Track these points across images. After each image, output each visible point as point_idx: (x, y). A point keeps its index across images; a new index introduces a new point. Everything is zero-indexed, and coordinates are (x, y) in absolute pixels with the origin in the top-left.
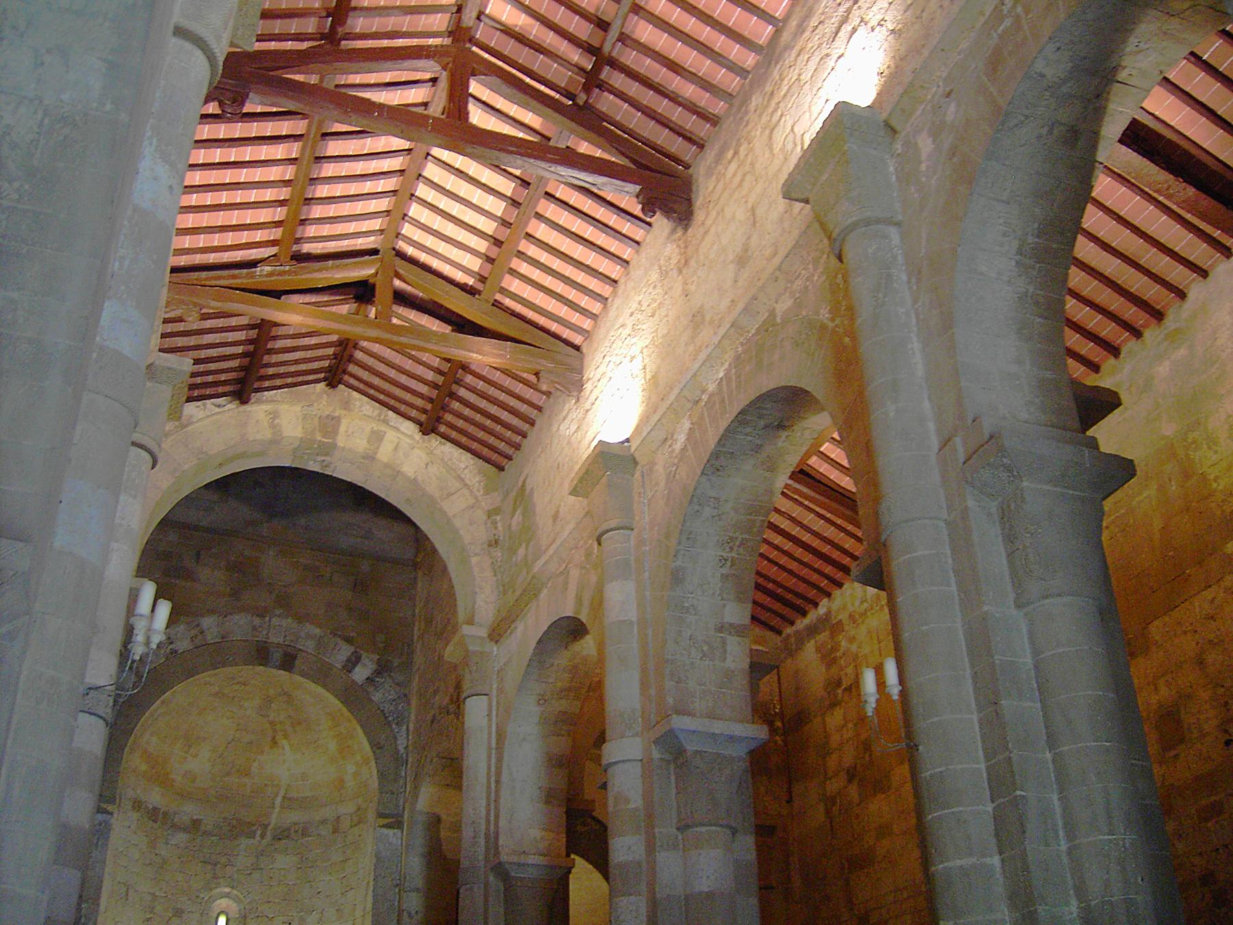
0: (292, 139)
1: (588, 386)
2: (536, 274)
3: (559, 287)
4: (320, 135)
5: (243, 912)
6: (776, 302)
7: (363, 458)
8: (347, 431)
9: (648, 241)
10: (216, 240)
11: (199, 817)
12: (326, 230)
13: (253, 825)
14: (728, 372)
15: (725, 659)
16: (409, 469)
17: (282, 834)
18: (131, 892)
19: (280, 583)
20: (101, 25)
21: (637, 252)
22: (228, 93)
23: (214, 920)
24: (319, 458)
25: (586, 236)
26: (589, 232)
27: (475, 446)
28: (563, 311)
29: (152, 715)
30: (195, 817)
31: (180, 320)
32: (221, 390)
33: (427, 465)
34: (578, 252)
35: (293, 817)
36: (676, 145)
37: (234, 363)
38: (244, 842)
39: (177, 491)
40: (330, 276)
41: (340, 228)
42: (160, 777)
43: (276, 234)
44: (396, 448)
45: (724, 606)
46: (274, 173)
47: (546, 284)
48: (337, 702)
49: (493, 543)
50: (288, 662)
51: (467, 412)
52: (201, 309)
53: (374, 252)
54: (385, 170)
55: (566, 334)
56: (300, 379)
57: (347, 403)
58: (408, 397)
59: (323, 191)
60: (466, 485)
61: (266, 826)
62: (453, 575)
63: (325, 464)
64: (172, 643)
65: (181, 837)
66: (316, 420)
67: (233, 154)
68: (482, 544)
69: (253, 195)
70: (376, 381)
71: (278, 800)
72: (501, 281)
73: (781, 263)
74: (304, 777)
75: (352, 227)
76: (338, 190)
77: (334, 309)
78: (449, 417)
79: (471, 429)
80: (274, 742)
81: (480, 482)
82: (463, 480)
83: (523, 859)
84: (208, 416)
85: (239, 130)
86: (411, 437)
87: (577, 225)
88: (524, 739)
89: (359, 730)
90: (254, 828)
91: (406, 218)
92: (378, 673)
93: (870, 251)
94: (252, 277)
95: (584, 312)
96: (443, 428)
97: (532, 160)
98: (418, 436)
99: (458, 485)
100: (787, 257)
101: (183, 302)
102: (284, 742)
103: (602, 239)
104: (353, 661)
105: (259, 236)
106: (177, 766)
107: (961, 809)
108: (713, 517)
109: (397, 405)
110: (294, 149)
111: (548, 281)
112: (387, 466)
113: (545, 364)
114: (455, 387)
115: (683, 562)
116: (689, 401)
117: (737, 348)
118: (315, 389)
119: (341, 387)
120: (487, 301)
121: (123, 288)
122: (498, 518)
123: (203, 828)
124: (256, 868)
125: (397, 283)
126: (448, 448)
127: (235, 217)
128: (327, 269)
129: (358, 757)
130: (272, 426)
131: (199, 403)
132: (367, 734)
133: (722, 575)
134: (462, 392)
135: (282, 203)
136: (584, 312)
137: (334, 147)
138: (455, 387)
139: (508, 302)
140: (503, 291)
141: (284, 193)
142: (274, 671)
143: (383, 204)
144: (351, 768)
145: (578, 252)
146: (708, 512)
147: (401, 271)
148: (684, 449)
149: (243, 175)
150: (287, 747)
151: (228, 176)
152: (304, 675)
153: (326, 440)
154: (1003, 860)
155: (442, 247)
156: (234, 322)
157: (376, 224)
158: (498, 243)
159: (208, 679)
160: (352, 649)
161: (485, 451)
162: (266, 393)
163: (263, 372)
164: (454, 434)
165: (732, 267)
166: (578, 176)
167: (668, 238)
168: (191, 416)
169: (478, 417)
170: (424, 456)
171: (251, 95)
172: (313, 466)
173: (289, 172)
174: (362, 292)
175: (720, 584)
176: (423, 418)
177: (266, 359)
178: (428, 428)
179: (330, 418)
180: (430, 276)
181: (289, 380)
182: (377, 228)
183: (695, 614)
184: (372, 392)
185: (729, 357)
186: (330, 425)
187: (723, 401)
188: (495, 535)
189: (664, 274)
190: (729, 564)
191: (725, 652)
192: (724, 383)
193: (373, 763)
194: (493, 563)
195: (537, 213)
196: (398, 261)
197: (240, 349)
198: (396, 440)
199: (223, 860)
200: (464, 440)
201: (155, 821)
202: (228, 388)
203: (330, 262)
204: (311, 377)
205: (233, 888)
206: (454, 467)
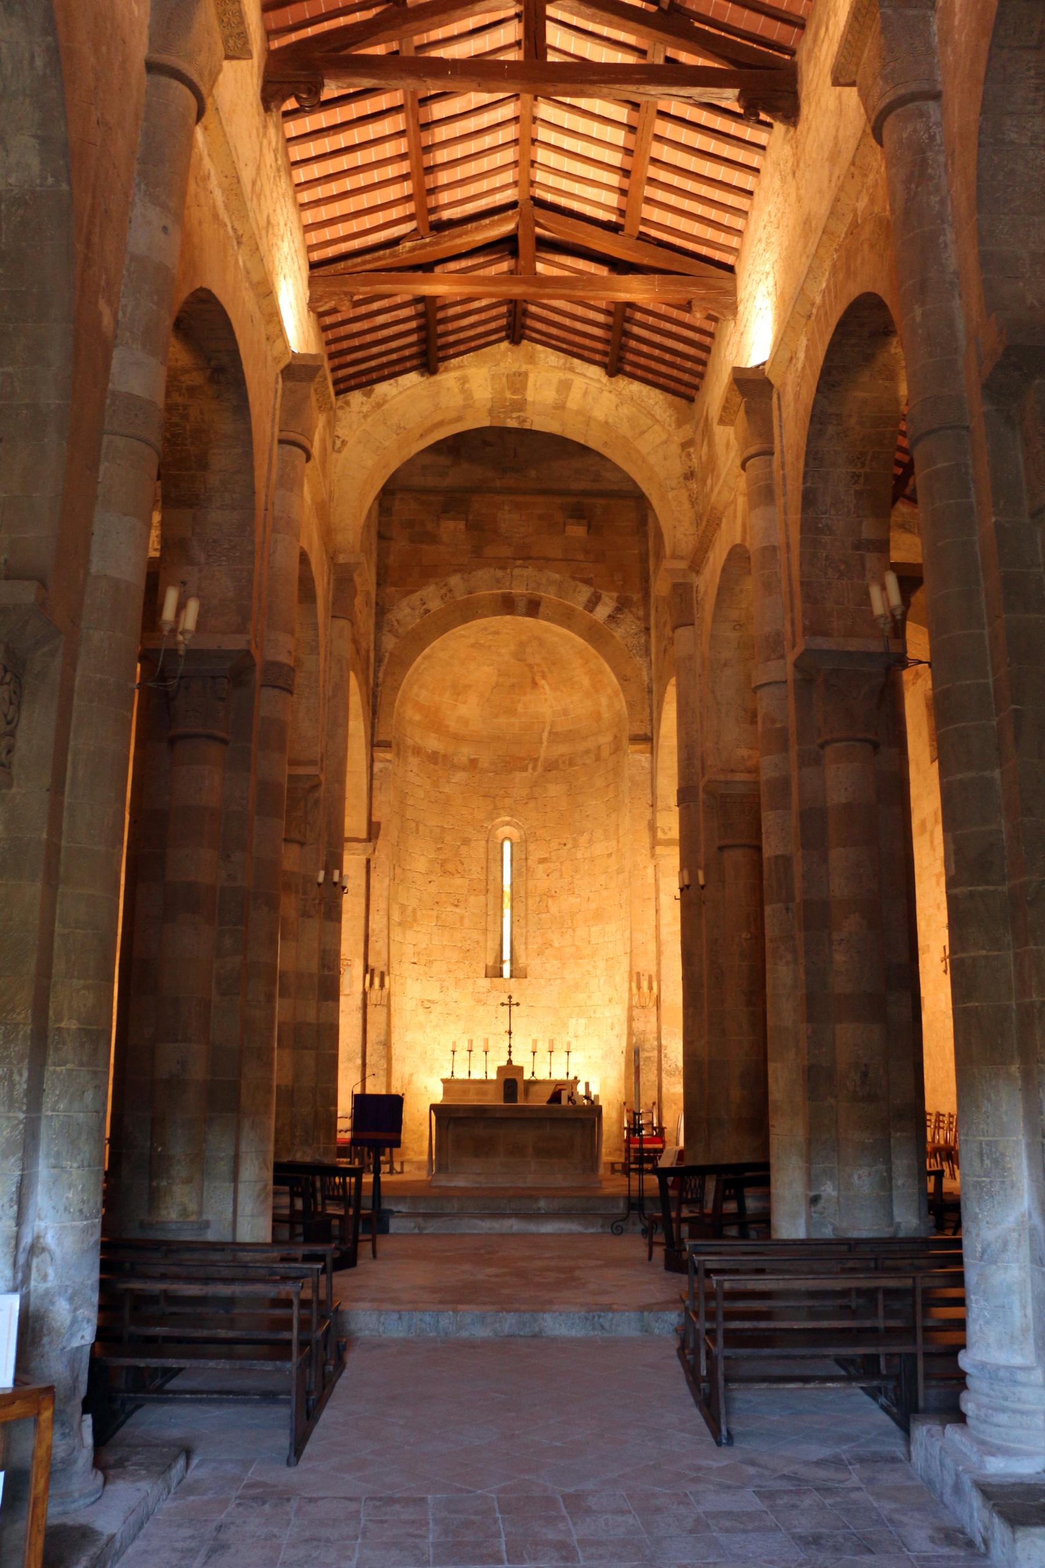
0: (393, 112)
1: (741, 308)
2: (672, 199)
3: (699, 209)
4: (417, 101)
5: (524, 837)
6: (857, 200)
7: (554, 408)
8: (535, 385)
9: (771, 143)
10: (355, 226)
11: (475, 756)
12: (459, 193)
13: (524, 760)
14: (828, 280)
15: (864, 575)
16: (599, 413)
17: (551, 766)
18: (421, 828)
19: (518, 535)
20: (22, 103)
21: (764, 157)
22: (302, 86)
23: (499, 846)
24: (515, 415)
25: (711, 151)
26: (712, 145)
27: (662, 380)
28: (709, 233)
29: (416, 670)
30: (472, 757)
31: (334, 311)
32: (408, 364)
33: (617, 406)
34: (707, 168)
35: (563, 749)
36: (776, 31)
37: (413, 338)
38: (519, 776)
39: (384, 467)
40: (470, 239)
41: (472, 189)
42: (435, 723)
43: (410, 208)
44: (585, 394)
45: (861, 522)
46: (389, 149)
47: (685, 208)
48: (582, 641)
49: (689, 476)
50: (533, 608)
51: (645, 348)
52: (352, 297)
53: (513, 205)
54: (500, 121)
55: (718, 255)
56: (482, 341)
57: (531, 357)
58: (587, 342)
59: (442, 156)
60: (658, 421)
61: (536, 760)
62: (657, 511)
63: (521, 419)
64: (424, 604)
65: (460, 776)
66: (504, 380)
67: (342, 140)
68: (678, 478)
69: (376, 176)
70: (554, 331)
71: (545, 735)
72: (640, 212)
73: (854, 157)
74: (565, 712)
75: (484, 185)
76: (459, 151)
77: (481, 272)
78: (630, 357)
79: (653, 364)
80: (535, 684)
81: (670, 416)
82: (653, 416)
83: (730, 777)
84: (401, 393)
85: (323, 119)
86: (599, 381)
87: (699, 141)
88: (725, 665)
89: (607, 668)
90: (527, 762)
91: (536, 165)
92: (618, 610)
93: (905, 135)
94: (395, 256)
95: (728, 230)
96: (628, 368)
97: (617, 86)
98: (605, 379)
99: (650, 422)
100: (857, 149)
101: (335, 293)
102: (543, 682)
103: (727, 150)
104: (592, 604)
105: (395, 213)
106: (448, 713)
107: (963, 724)
108: (838, 434)
109: (580, 351)
110: (399, 122)
111: (686, 204)
112: (579, 412)
113: (695, 292)
114: (627, 326)
115: (812, 484)
116: (802, 316)
117: (833, 255)
118: (499, 349)
119: (525, 342)
120: (631, 236)
121: (128, 334)
122: (692, 450)
123: (480, 765)
124: (532, 797)
125: (538, 230)
126: (636, 387)
127: (365, 201)
128: (466, 233)
129: (609, 691)
130: (463, 391)
131: (392, 381)
132: (613, 669)
133: (856, 492)
134: (636, 330)
135: (404, 177)
136: (728, 230)
137: (439, 110)
138: (627, 326)
139: (653, 233)
140: (645, 222)
141: (404, 167)
142: (520, 618)
143: (509, 155)
144: (604, 701)
145: (707, 168)
146: (831, 430)
147: (541, 221)
148: (804, 368)
149: (359, 158)
150: (547, 687)
151: (344, 162)
152: (548, 619)
153: (515, 397)
154: (1002, 773)
155: (577, 188)
156: (398, 300)
157: (509, 176)
158: (626, 173)
159: (462, 632)
160: (592, 589)
161: (672, 384)
162: (453, 361)
163: (441, 342)
164: (639, 373)
165: (827, 164)
166: (670, 92)
167: (784, 138)
168: (386, 395)
169: (657, 352)
170: (612, 397)
171: (326, 81)
172: (512, 423)
173: (402, 146)
174: (508, 246)
175: (855, 502)
176: (607, 360)
177: (441, 329)
178: (614, 369)
179: (517, 375)
180: (571, 221)
181: (473, 344)
182: (511, 181)
183: (830, 535)
184: (554, 342)
185: (827, 265)
186: (518, 381)
187: (826, 313)
188: (690, 467)
189: (783, 179)
190: (862, 480)
191: (864, 567)
192: (826, 294)
193: (621, 695)
194: (690, 495)
195: (656, 135)
196: (538, 212)
197: (413, 324)
198: (584, 386)
199: (502, 792)
200: (650, 376)
201: (436, 764)
202: (415, 362)
203: (469, 226)
204: (493, 337)
205: (512, 816)
206: (643, 404)
